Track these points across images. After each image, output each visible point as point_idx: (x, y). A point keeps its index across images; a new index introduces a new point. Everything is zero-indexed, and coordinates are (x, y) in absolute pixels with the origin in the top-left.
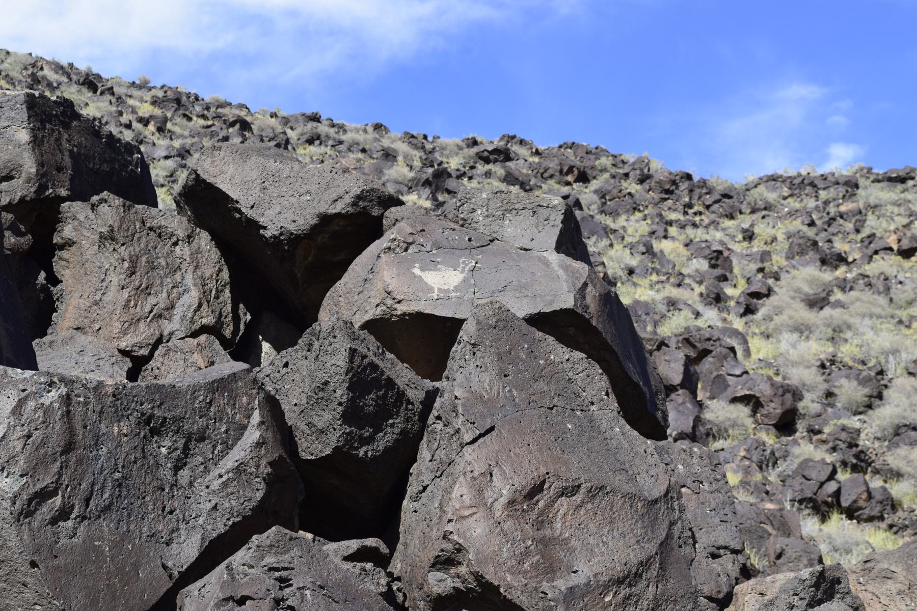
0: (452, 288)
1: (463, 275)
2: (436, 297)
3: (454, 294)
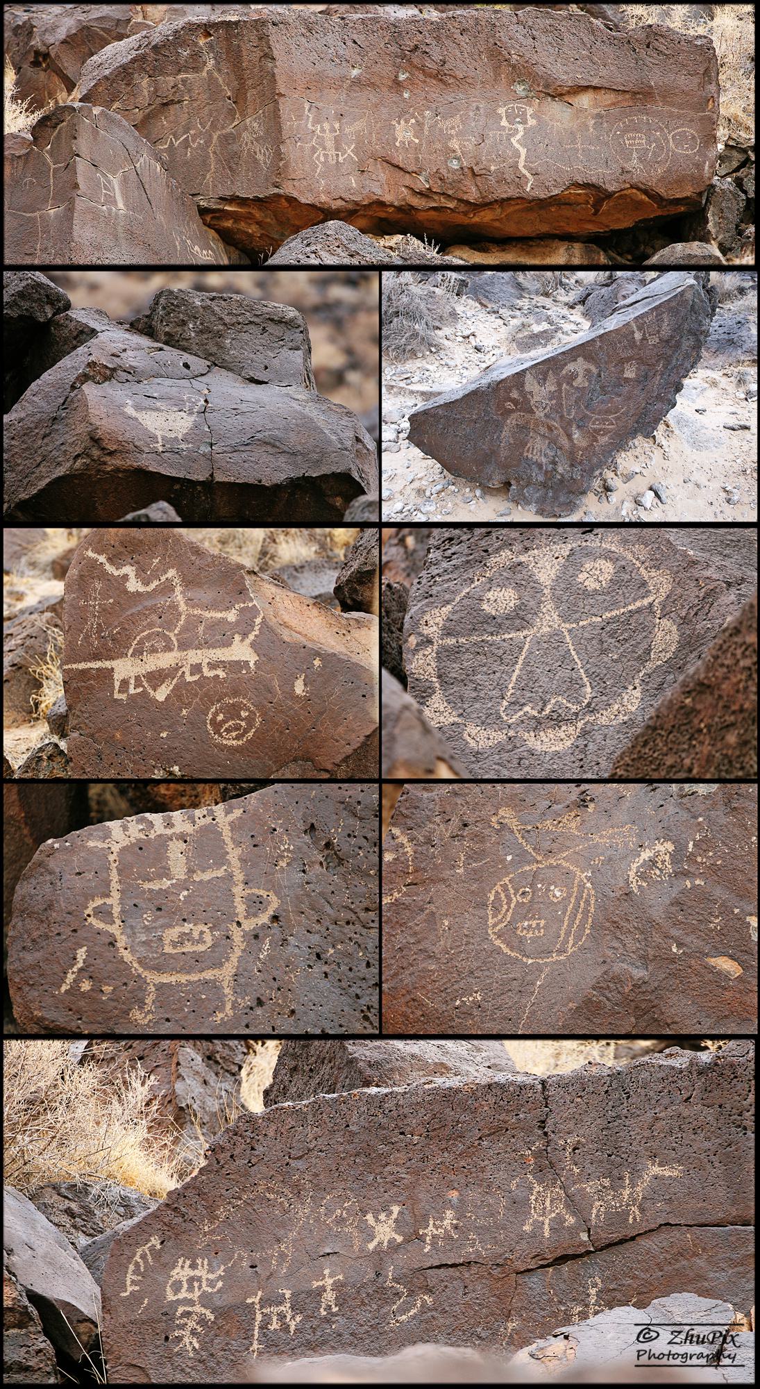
0: (180, 437)
1: (193, 418)
2: (161, 449)
3: (184, 446)
